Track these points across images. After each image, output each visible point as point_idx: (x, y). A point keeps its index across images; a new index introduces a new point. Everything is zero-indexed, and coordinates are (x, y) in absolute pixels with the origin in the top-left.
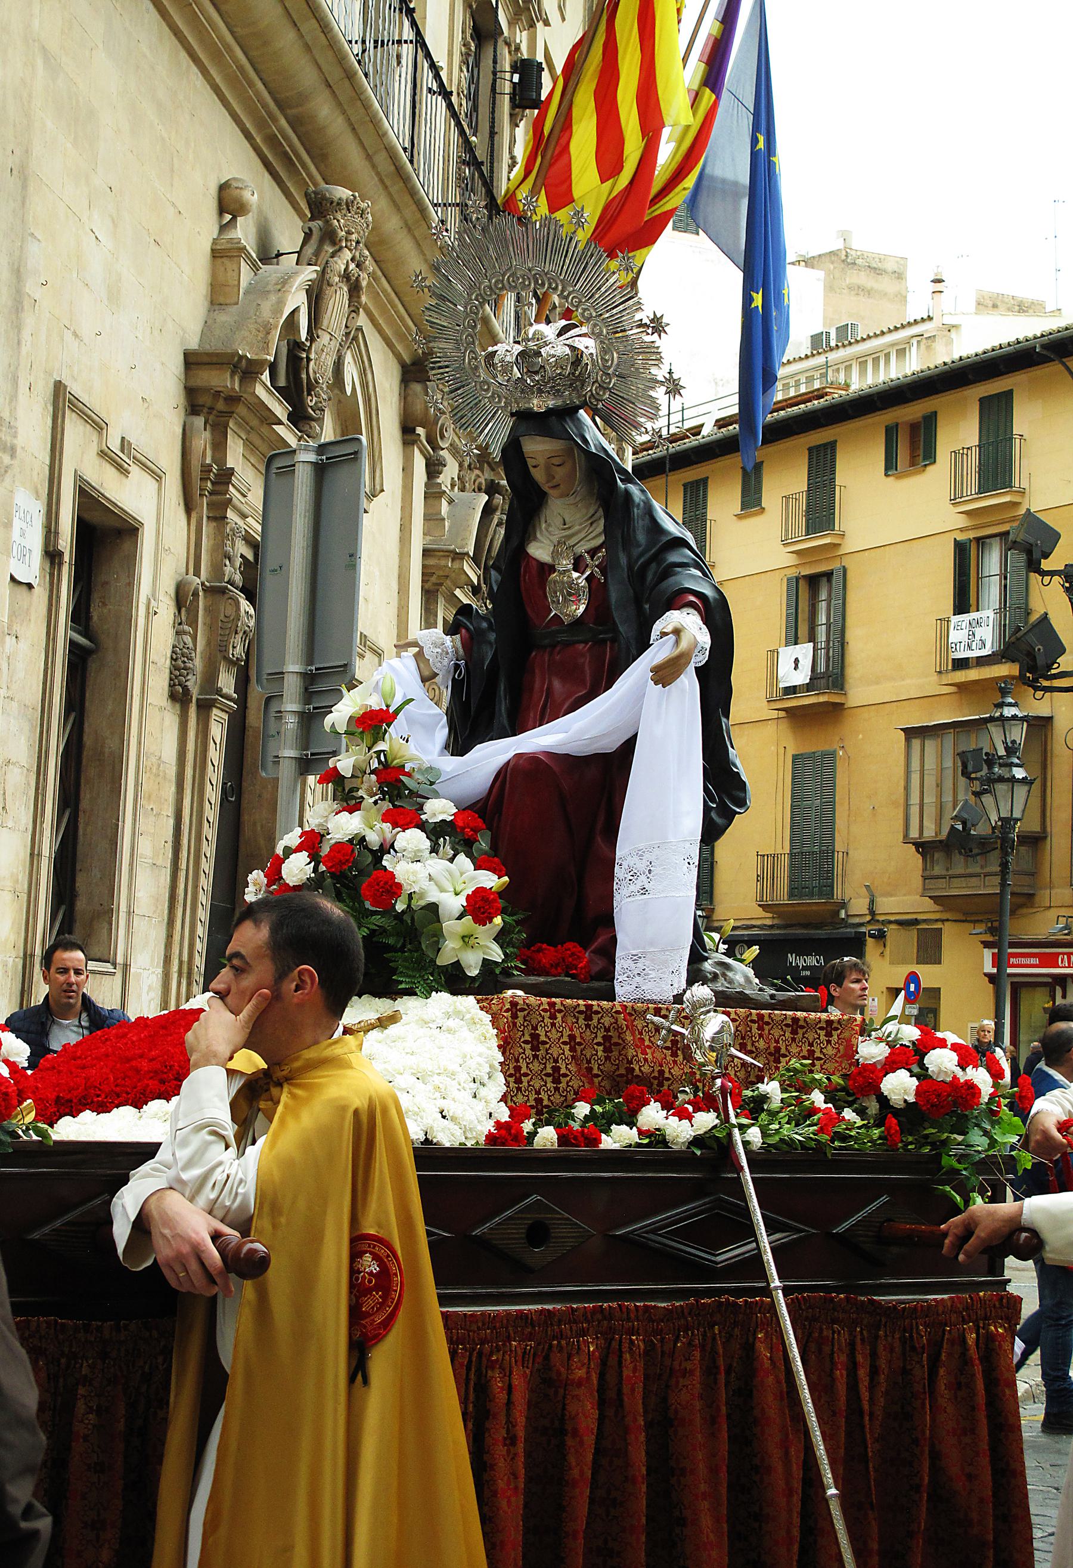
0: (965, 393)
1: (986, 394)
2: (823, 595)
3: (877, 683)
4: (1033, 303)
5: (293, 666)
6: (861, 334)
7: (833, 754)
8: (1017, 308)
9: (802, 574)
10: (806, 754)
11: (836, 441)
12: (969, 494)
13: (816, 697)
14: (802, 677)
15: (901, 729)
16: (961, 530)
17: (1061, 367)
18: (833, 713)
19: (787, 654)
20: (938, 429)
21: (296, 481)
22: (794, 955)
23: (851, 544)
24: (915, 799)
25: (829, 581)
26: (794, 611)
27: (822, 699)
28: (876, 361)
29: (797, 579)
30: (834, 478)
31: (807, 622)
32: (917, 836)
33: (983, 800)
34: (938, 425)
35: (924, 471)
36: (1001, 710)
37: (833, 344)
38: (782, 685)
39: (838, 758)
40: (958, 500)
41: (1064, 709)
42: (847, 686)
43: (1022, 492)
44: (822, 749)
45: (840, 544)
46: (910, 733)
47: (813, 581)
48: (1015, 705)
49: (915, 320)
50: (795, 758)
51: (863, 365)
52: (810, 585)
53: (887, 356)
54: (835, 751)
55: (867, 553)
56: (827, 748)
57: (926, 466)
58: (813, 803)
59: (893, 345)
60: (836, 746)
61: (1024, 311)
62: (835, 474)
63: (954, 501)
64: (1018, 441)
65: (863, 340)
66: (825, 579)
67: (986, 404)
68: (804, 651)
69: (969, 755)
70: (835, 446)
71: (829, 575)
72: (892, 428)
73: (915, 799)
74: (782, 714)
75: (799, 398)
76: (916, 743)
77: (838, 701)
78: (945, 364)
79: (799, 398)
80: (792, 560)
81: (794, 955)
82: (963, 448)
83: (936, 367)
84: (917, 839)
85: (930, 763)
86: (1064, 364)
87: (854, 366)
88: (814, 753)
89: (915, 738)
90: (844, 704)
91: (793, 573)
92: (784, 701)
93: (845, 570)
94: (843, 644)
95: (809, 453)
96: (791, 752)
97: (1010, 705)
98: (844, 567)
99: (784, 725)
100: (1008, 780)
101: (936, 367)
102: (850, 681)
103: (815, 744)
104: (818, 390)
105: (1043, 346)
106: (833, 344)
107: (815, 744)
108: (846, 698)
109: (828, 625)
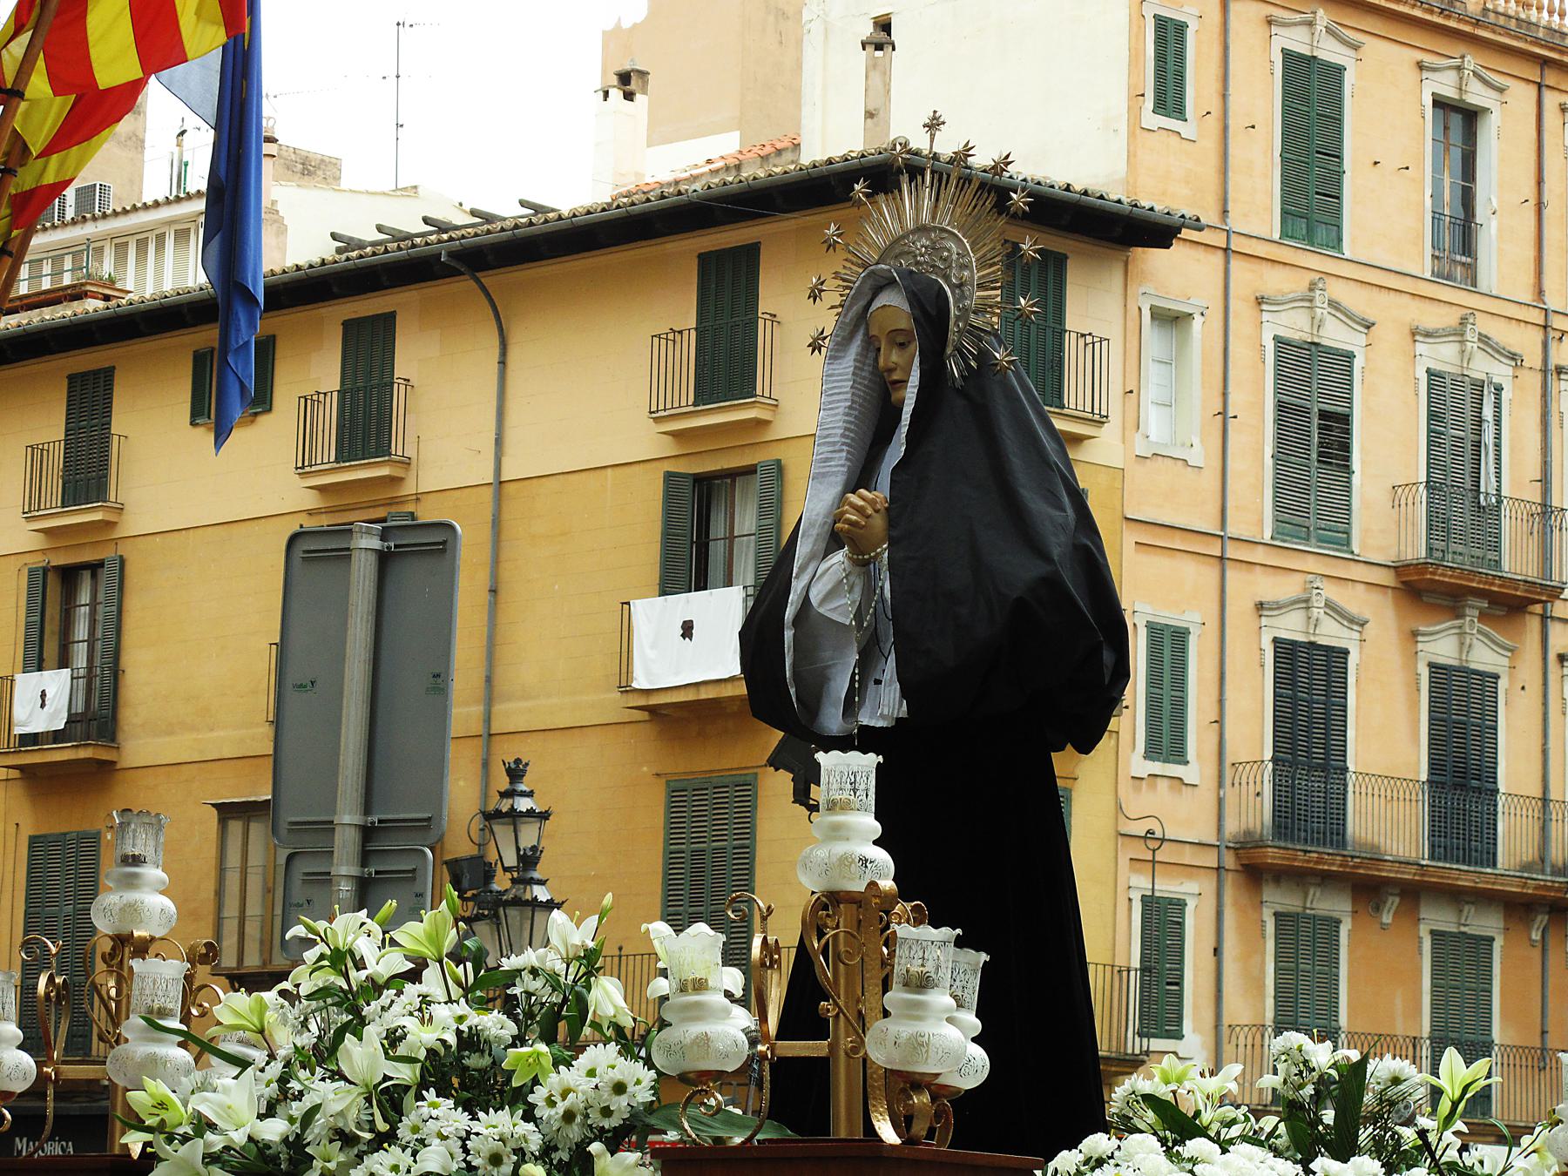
0: (323, 311)
1: (354, 316)
2: (84, 597)
3: (171, 733)
4: (322, 161)
5: (348, 816)
6: (115, 206)
7: (96, 837)
8: (300, 167)
9: (52, 564)
10: (50, 835)
11: (114, 367)
12: (326, 460)
13: (74, 751)
14: (53, 718)
15: (213, 805)
16: (310, 513)
17: (472, 283)
18: (100, 775)
19: (27, 685)
20: (276, 362)
21: (353, 567)
22: (25, 1140)
23: (136, 522)
24: (231, 910)
25: (94, 576)
26: (37, 618)
27: (83, 754)
28: (142, 246)
29: (45, 570)
30: (109, 424)
31: (57, 637)
32: (234, 965)
33: (474, 927)
34: (277, 356)
35: (252, 422)
36: (510, 801)
37: (69, 217)
38: (17, 731)
39: (103, 842)
40: (308, 469)
41: (461, 783)
42: (121, 737)
43: (406, 463)
44: (78, 829)
45: (116, 523)
46: (227, 812)
47: (69, 576)
48: (530, 794)
49: (199, 191)
50: (34, 841)
51: (121, 249)
52: (63, 579)
53: (161, 239)
54: (99, 833)
55: (158, 539)
56: (86, 827)
57: (256, 414)
58: (61, 910)
59: (170, 222)
60: (99, 825)
61: (310, 174)
62: (110, 416)
63: (302, 470)
64: (402, 388)
65: (115, 214)
66: (87, 575)
67: (352, 329)
68: (57, 683)
69: (465, 864)
70: (113, 376)
71: (95, 567)
72: (204, 354)
73: (231, 910)
74: (15, 774)
75: (43, 297)
76: (235, 827)
77: (104, 757)
78: (298, 268)
79: (43, 297)
80: (38, 542)
81: (25, 1140)
82: (319, 393)
83: (284, 272)
84: (234, 969)
85: (257, 857)
86: (478, 281)
87: (107, 251)
88: (65, 834)
89: (233, 818)
90: (113, 763)
91: (38, 561)
92: (21, 755)
93: (122, 561)
94: (116, 672)
95: (69, 383)
96: (27, 831)
97: (524, 794)
98: (121, 557)
99: (18, 790)
100: (527, 903)
101: (284, 272)
102: (126, 728)
103: (66, 821)
104: (68, 287)
105: (451, 254)
106: (69, 217)
107: (66, 821)
108: (120, 755)
109: (91, 642)
